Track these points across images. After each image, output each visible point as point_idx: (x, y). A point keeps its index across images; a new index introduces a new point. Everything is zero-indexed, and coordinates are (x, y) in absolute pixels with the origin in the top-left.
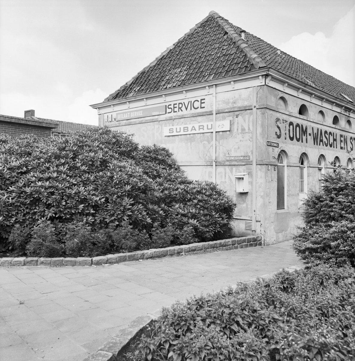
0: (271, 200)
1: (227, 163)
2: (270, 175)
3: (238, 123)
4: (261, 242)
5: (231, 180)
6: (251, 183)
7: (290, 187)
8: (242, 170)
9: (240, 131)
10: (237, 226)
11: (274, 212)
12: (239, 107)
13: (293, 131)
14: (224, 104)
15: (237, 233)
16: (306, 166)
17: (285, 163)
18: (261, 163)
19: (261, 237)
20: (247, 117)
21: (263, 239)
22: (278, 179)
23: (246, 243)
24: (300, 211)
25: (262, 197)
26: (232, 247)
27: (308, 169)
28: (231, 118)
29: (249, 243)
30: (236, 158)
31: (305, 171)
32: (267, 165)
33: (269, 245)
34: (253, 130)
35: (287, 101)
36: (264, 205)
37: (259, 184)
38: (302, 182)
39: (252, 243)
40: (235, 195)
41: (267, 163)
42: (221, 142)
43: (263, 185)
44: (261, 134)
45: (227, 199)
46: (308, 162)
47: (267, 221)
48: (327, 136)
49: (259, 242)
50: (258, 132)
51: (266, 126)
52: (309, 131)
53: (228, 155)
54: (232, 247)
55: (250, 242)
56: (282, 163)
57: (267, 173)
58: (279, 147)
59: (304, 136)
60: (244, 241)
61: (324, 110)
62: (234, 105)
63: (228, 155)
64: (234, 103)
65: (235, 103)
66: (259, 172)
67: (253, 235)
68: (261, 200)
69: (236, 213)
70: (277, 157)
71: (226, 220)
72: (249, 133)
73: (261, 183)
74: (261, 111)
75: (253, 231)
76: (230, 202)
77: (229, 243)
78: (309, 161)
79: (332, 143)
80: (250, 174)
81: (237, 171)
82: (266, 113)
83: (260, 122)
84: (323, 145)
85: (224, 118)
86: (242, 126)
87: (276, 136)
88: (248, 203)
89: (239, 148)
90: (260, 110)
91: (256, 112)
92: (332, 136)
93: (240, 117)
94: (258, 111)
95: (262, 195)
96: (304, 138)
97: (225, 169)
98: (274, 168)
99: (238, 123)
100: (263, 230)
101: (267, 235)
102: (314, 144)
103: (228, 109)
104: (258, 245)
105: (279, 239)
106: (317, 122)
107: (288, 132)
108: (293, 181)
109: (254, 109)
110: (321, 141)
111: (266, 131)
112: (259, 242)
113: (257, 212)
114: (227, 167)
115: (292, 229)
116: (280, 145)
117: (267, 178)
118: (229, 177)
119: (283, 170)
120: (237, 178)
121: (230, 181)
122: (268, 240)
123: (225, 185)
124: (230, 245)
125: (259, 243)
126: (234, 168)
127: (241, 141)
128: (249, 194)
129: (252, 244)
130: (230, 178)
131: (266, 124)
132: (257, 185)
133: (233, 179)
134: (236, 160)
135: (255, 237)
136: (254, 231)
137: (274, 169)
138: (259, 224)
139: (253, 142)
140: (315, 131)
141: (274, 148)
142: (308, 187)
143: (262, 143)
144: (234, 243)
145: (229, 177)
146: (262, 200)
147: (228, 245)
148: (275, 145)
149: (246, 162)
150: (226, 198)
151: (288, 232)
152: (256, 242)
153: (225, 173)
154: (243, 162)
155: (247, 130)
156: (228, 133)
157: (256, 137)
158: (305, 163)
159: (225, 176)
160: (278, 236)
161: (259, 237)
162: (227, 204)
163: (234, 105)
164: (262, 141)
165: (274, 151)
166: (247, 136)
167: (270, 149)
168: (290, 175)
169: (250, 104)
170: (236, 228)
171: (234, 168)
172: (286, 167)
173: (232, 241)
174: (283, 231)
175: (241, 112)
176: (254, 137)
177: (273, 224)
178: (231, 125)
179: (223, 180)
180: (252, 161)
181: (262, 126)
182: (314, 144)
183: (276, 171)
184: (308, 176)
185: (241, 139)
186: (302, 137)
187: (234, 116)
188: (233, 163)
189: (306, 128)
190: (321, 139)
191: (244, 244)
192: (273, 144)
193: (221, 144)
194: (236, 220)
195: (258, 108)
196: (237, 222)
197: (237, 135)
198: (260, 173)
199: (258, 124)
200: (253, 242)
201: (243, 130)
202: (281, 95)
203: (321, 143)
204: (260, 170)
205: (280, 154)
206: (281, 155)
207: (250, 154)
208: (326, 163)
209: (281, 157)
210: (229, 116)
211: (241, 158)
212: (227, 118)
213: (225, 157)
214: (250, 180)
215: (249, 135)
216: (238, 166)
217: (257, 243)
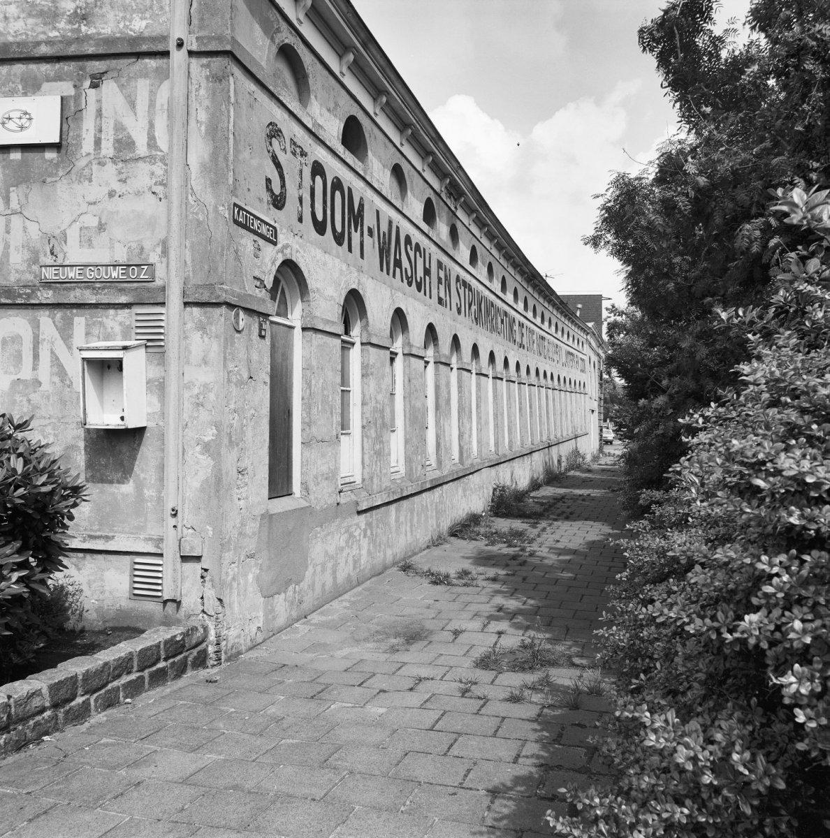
0: (246, 463)
1: (46, 296)
2: (242, 355)
3: (99, 113)
4: (205, 651)
5: (61, 372)
6: (158, 387)
7: (314, 411)
8: (118, 329)
9: (108, 149)
10: (92, 584)
11: (258, 511)
12: (108, 41)
13: (325, 202)
14: (31, 21)
15: (95, 615)
16: (358, 341)
17: (295, 318)
18: (205, 298)
19: (206, 629)
20: (142, 88)
21: (212, 637)
22: (272, 377)
23: (133, 677)
24: (342, 501)
25: (207, 448)
26: (55, 717)
27: (362, 351)
28: (67, 88)
29: (146, 673)
30: (90, 275)
31: (355, 354)
32: (231, 306)
33: (239, 653)
34: (171, 147)
35: (305, 76)
36: (217, 486)
37: (196, 391)
38: (345, 393)
39: (161, 665)
40: (82, 444)
41: (233, 300)
42: (13, 196)
43: (212, 396)
44: (204, 168)
45: (26, 462)
46: (365, 327)
47: (228, 556)
48: (412, 254)
49: (195, 652)
50: (193, 160)
51: (231, 136)
52: (369, 220)
53: (49, 260)
54: (55, 717)
55: (154, 664)
56: (283, 312)
57: (233, 344)
58: (279, 246)
59: (356, 231)
60: (124, 666)
61: (406, 168)
62: (83, 28)
63: (49, 260)
64: (83, 16)
65: (84, 17)
66: (196, 337)
67: (167, 622)
68: (206, 462)
69: (81, 524)
70: (269, 282)
71: (15, 576)
72: (151, 159)
73: (205, 386)
74: (208, 66)
75: (165, 602)
76: (44, 478)
77: (36, 702)
78: (367, 324)
79: (421, 278)
80: (154, 346)
81: (95, 331)
82: (231, 78)
83: (203, 116)
84: (402, 281)
85: (32, 86)
86: (119, 127)
87: (266, 197)
88: (142, 475)
89: (101, 227)
90: (205, 61)
91: (184, 67)
92: (421, 256)
93: (109, 88)
94: (195, 62)
95: (206, 439)
96: (356, 237)
97: (36, 325)
98: (261, 325)
99: (99, 113)
100: (210, 594)
101: (228, 613)
102: (382, 270)
103: (49, 42)
104: (189, 667)
105: (274, 618)
106: (389, 198)
107: (307, 197)
108: (323, 389)
109: (178, 57)
110: (398, 263)
111: (231, 158)
112: (195, 652)
113: (186, 516)
114: (44, 317)
115: (319, 568)
116: (282, 239)
117: (231, 366)
118: (56, 361)
119: (289, 346)
120: (89, 362)
121: (56, 379)
122: (233, 635)
123: (32, 396)
124: (43, 710)
125: (195, 658)
126: (80, 321)
127: (111, 194)
128: (147, 434)
129: (163, 670)
130: (60, 366)
131: (231, 127)
132: (187, 394)
133: (74, 367)
134: (88, 284)
135: (176, 632)
136: (173, 601)
137: (261, 329)
138: (193, 569)
139: (170, 203)
140: (384, 228)
141: (261, 242)
142: (363, 413)
143: (211, 209)
144: (63, 694)
145: (56, 361)
146: (212, 463)
147: (23, 719)
148: (264, 230)
149: (136, 291)
150: (20, 455)
151: (304, 585)
152: (185, 655)
153: (36, 343)
154: (121, 290)
155: (142, 149)
156: (50, 155)
157: (186, 179)
158: (356, 331)
159: (36, 356)
160: (272, 611)
161: (194, 629)
162: (21, 491)
163: (83, 28)
164: (209, 199)
165: (260, 254)
166: (142, 176)
167: (243, 241)
168: (314, 363)
169: (157, 31)
170: (87, 592)
171: (76, 319)
172: (297, 332)
173: (55, 688)
174: (288, 583)
175: (113, 63)
176: (175, 182)
177: (252, 561)
178: (64, 119)
179: (26, 373)
180: (163, 289)
181: (215, 132)
182: (382, 270)
183: (268, 341)
184: (363, 376)
185: (116, 186)
186: (350, 233)
187: (81, 79)
188: (72, 294)
189: (361, 206)
190: (398, 257)
191: (125, 679)
192: (256, 223)
193: (14, 204)
194: (88, 556)
195: (194, 48)
196: (90, 563)
197: (95, 167)
198: (198, 345)
199: (192, 123)
200: (166, 660)
201: (124, 144)
202: (291, 39)
203: (398, 270)
204: (202, 327)
205: (280, 278)
206: (283, 282)
207: (154, 258)
208: (408, 338)
209: (283, 289)
210: (58, 78)
211: (115, 274)
212: (46, 86)
213: (35, 268)
214: (155, 372)
215: (154, 168)
216: (100, 311)
217: (186, 658)
